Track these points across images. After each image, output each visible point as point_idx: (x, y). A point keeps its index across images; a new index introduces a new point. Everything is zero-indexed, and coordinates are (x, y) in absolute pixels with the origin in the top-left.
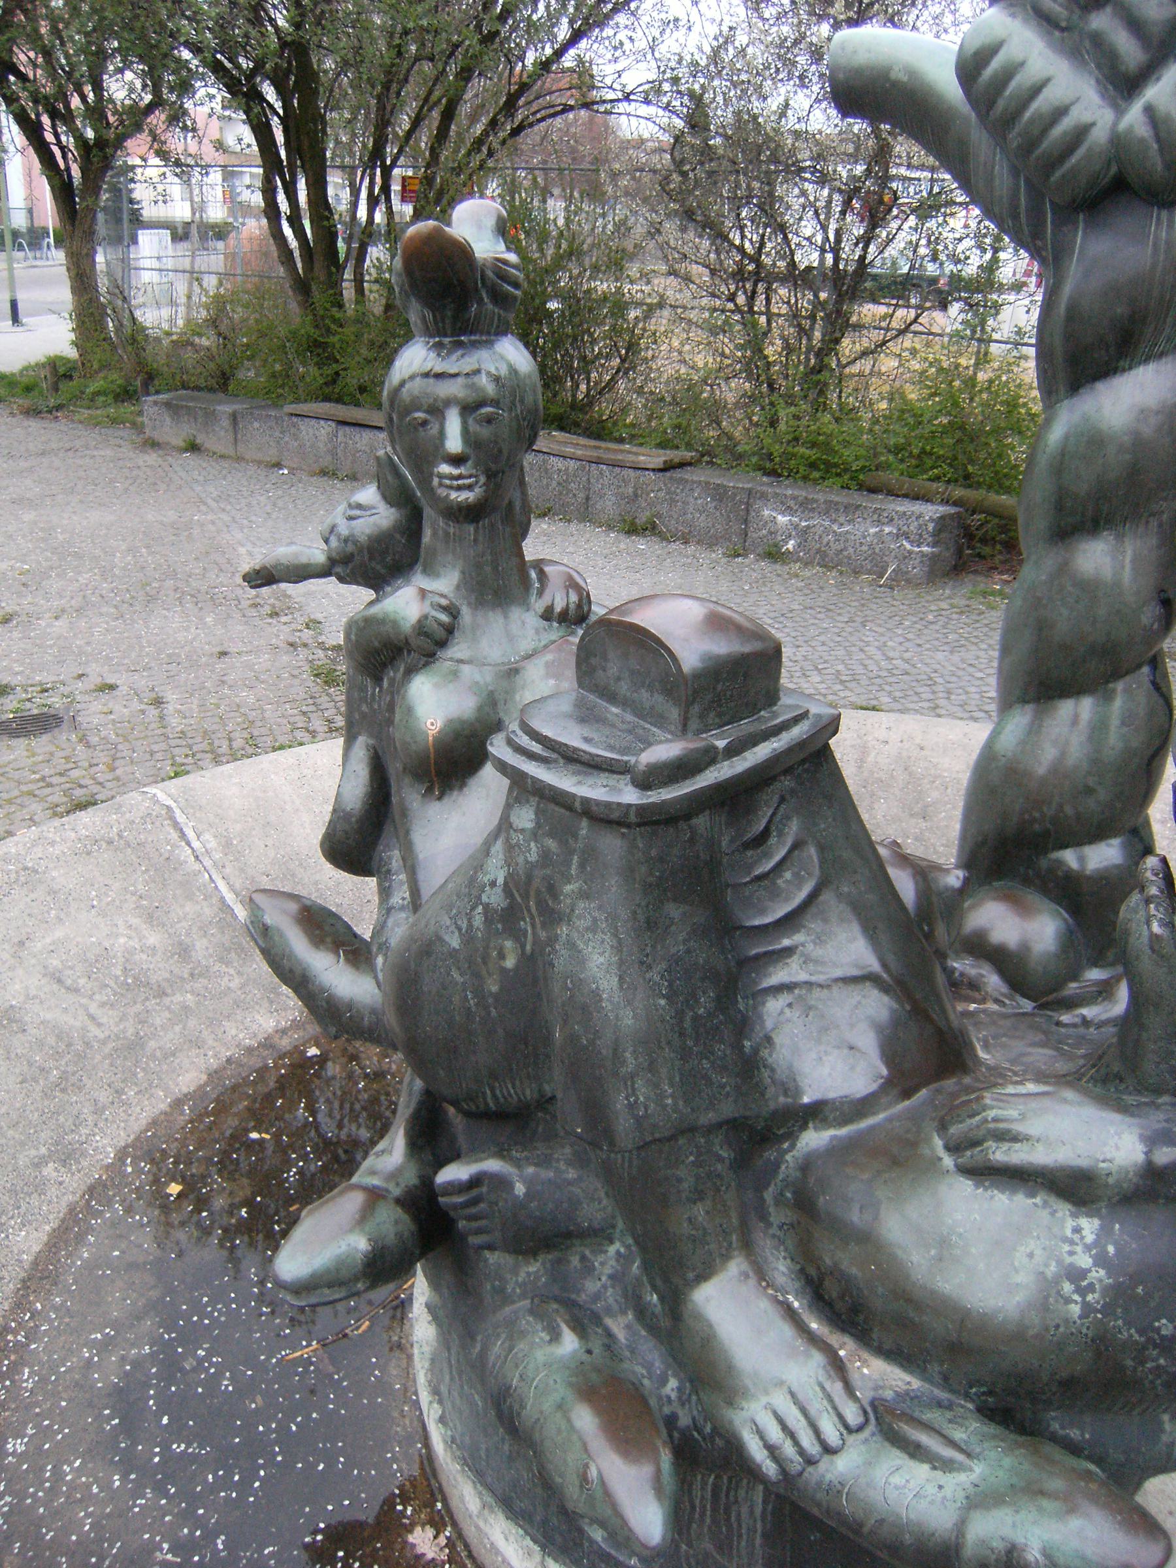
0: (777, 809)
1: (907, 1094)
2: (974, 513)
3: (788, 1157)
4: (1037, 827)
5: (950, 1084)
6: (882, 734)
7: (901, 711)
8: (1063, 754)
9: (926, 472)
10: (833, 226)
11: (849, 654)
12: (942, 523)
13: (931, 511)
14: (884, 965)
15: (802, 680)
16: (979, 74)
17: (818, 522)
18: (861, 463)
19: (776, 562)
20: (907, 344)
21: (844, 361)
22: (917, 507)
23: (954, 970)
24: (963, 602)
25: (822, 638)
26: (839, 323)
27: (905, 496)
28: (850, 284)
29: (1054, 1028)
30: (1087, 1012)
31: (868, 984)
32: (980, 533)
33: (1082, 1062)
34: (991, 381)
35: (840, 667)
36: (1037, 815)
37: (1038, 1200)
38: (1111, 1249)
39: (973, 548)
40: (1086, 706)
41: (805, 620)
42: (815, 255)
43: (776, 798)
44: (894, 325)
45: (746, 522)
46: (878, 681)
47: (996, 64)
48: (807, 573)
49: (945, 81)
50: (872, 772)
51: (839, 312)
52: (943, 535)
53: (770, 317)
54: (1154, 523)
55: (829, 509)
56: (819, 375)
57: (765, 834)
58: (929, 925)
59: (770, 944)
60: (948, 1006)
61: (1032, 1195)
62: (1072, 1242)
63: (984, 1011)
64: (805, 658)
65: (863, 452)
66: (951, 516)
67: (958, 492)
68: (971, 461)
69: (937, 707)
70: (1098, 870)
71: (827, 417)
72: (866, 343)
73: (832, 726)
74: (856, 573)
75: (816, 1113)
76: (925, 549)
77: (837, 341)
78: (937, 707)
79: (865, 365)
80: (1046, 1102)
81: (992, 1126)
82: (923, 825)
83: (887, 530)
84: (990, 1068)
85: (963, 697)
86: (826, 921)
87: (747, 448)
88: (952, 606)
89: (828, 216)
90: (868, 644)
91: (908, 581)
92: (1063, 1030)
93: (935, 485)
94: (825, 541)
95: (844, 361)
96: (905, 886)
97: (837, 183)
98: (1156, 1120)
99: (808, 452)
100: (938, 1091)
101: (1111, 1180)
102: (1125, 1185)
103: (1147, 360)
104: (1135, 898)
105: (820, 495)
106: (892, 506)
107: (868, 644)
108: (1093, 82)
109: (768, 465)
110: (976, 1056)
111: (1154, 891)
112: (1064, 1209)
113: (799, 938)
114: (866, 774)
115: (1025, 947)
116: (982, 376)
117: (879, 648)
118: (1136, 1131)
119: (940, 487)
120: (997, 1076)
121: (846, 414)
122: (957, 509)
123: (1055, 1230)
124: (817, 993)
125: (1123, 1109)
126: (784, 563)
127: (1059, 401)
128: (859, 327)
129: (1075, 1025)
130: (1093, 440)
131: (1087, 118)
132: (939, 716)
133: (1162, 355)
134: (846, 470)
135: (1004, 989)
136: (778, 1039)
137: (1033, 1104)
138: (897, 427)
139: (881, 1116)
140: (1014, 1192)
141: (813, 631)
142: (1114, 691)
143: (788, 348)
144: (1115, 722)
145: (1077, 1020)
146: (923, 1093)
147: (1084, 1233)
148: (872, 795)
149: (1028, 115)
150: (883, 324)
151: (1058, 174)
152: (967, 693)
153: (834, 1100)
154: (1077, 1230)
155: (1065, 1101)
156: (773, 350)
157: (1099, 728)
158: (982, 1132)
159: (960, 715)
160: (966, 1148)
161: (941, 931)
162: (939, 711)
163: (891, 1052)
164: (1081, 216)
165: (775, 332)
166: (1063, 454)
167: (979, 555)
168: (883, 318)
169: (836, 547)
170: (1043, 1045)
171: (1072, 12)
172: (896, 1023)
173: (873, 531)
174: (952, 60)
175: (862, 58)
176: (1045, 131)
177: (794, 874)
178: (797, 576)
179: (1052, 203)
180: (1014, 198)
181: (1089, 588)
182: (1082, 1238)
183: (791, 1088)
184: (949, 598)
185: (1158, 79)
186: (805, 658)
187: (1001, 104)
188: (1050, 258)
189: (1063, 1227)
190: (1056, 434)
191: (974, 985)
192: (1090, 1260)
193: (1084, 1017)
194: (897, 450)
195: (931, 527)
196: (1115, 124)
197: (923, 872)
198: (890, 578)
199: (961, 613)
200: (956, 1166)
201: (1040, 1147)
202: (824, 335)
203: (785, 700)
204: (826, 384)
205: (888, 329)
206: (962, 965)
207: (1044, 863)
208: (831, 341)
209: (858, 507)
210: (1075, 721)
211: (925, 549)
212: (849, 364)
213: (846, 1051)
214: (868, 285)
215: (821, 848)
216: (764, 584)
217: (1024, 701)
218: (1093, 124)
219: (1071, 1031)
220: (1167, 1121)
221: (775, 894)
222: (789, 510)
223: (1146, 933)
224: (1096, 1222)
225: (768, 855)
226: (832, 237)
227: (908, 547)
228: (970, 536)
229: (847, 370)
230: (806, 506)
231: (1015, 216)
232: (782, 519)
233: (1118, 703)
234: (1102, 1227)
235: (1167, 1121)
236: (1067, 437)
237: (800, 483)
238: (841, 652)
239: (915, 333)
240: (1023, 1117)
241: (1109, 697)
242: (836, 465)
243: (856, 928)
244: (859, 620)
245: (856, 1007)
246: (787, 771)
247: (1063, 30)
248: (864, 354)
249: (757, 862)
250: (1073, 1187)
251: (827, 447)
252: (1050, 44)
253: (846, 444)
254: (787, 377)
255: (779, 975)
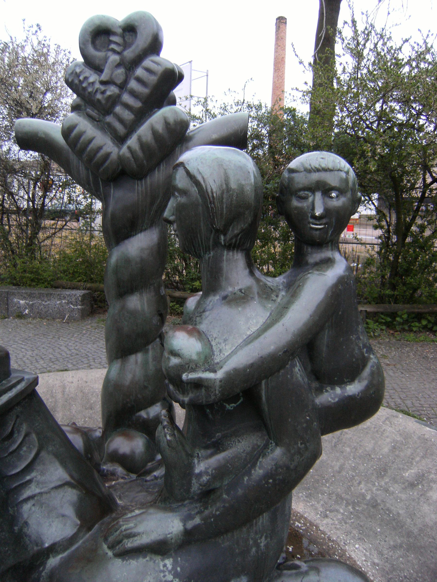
0: (15, 421)
1: (89, 529)
2: (95, 291)
3: (43, 574)
4: (129, 405)
5: (107, 519)
6: (70, 379)
7: (77, 369)
8: (134, 376)
9: (76, 279)
10: (31, 193)
11: (54, 350)
12: (84, 296)
13: (79, 293)
14: (72, 476)
15: (36, 364)
16: (70, 135)
17: (37, 302)
18: (51, 278)
19: (22, 318)
20: (64, 234)
21: (40, 241)
22: (74, 292)
23: (104, 470)
24: (96, 325)
25: (43, 346)
26: (37, 228)
27: (69, 288)
28: (38, 214)
29: (145, 483)
30: (155, 473)
31: (66, 487)
32: (99, 299)
33: (156, 494)
34: (96, 245)
35: (51, 356)
36: (128, 400)
37: (148, 558)
38: (179, 569)
39: (97, 304)
40: (139, 357)
41: (35, 340)
42: (25, 203)
43: (14, 417)
44: (58, 227)
45: (7, 304)
46: (67, 359)
47: (75, 132)
48: (35, 321)
49: (58, 137)
50: (69, 395)
51: (37, 223)
52: (85, 301)
53: (10, 226)
54: (152, 287)
55: (40, 296)
56: (32, 245)
57: (12, 433)
58: (91, 454)
59: (21, 480)
60: (101, 486)
61: (145, 557)
62: (164, 572)
63: (118, 484)
64: (37, 355)
65: (51, 273)
66: (87, 294)
67: (89, 285)
68: (92, 274)
69: (90, 365)
70: (154, 416)
71: (37, 262)
72: (48, 234)
73: (35, 382)
74: (54, 319)
75: (53, 549)
76: (79, 307)
77: (37, 233)
78: (90, 365)
79: (48, 242)
80: (144, 516)
81: (124, 533)
82: (91, 412)
83: (64, 301)
84: (122, 507)
85: (100, 360)
86: (44, 464)
87: (6, 276)
88: (92, 327)
89: (29, 188)
90: (61, 345)
91: (74, 320)
92: (148, 483)
93: (80, 283)
94: (40, 308)
95: (40, 241)
96: (77, 441)
97: (31, 177)
98: (185, 511)
99: (30, 275)
100: (102, 524)
101: (173, 541)
102: (179, 541)
103: (141, 231)
104: (160, 427)
105: (36, 291)
106: (64, 293)
107: (61, 345)
108: (109, 139)
109: (15, 282)
110: (116, 503)
111: (165, 423)
112: (158, 558)
113: (33, 474)
114: (66, 396)
115: (133, 452)
116: (93, 243)
117: (66, 346)
118: (178, 518)
119: (82, 284)
120: (127, 509)
121: (43, 260)
122: (89, 291)
123: (157, 569)
124: (45, 496)
125: (172, 510)
126: (25, 318)
127: (112, 248)
128: (45, 228)
129: (152, 480)
130: (126, 261)
131: (109, 150)
132: (92, 369)
133: (145, 230)
134: (45, 281)
135: (125, 472)
136: (30, 522)
137: (139, 519)
138: (63, 263)
139: (81, 542)
140: (138, 558)
141: (39, 344)
142: (148, 349)
143: (18, 238)
144: (150, 360)
145: (153, 478)
146: (97, 526)
147: (167, 566)
148: (70, 403)
149: (89, 149)
150: (54, 227)
151: (101, 169)
152: (101, 358)
153: (59, 542)
154: (165, 566)
155: (151, 514)
156: (13, 238)
157: (146, 363)
158: (121, 537)
159: (99, 367)
160: (117, 545)
161: (96, 456)
162: (91, 367)
163: (80, 514)
164: (112, 184)
165: (12, 232)
166: (117, 266)
167: (100, 307)
168: (53, 225)
169: (44, 310)
170: (141, 491)
171: (100, 115)
172: (81, 499)
173: (58, 302)
174: (60, 130)
175: (27, 129)
176: (95, 155)
177: (27, 448)
178: (30, 323)
179: (101, 179)
180: (88, 177)
181: (134, 313)
182: (167, 568)
183: (39, 542)
184: (91, 324)
185: (131, 138)
186: (37, 355)
187: (79, 146)
188: (104, 200)
189: (159, 567)
190: (114, 259)
191: (113, 474)
192: (172, 577)
193: (155, 476)
194: (65, 271)
195: (80, 298)
196: (119, 152)
197: (85, 433)
198: (67, 319)
199: (96, 329)
200: (113, 554)
201: (144, 536)
202: (31, 232)
203: (13, 375)
204: (34, 250)
205: (56, 228)
206: (107, 467)
207: (134, 418)
208: (34, 234)
209: (51, 294)
210: (136, 362)
211: (79, 307)
212: (42, 242)
213: (61, 518)
214: (46, 213)
215: (38, 434)
216: (17, 328)
217: (117, 358)
218: (112, 152)
219: (152, 482)
220: (189, 510)
221: (20, 458)
222: (24, 298)
223: (166, 440)
224: (171, 560)
225: (14, 442)
226: (31, 196)
227: (73, 307)
228: (95, 301)
229: (42, 244)
230: (31, 296)
231: (89, 184)
232: (22, 302)
233: (150, 353)
234: (174, 561)
235: (189, 510)
236: (117, 260)
237: (28, 287)
238: (51, 351)
239: (66, 229)
240: (136, 525)
241: (147, 352)
242: (42, 279)
243: (57, 464)
244: (57, 337)
245: (62, 498)
246: (18, 404)
247: (97, 121)
248: (48, 238)
249: (11, 445)
250: (159, 548)
251: (37, 273)
252: (94, 126)
253: (45, 271)
254: (19, 248)
255: (27, 493)
